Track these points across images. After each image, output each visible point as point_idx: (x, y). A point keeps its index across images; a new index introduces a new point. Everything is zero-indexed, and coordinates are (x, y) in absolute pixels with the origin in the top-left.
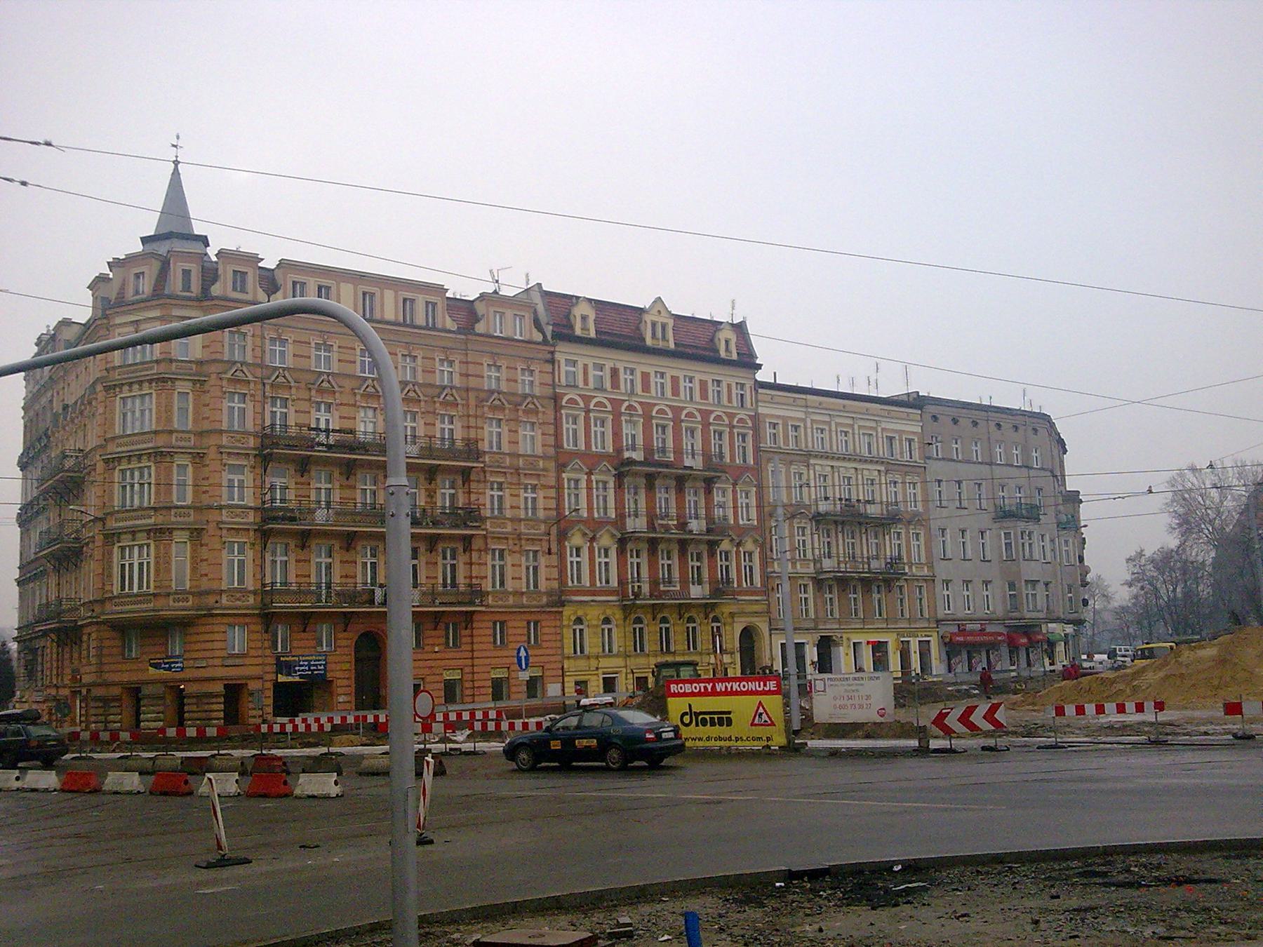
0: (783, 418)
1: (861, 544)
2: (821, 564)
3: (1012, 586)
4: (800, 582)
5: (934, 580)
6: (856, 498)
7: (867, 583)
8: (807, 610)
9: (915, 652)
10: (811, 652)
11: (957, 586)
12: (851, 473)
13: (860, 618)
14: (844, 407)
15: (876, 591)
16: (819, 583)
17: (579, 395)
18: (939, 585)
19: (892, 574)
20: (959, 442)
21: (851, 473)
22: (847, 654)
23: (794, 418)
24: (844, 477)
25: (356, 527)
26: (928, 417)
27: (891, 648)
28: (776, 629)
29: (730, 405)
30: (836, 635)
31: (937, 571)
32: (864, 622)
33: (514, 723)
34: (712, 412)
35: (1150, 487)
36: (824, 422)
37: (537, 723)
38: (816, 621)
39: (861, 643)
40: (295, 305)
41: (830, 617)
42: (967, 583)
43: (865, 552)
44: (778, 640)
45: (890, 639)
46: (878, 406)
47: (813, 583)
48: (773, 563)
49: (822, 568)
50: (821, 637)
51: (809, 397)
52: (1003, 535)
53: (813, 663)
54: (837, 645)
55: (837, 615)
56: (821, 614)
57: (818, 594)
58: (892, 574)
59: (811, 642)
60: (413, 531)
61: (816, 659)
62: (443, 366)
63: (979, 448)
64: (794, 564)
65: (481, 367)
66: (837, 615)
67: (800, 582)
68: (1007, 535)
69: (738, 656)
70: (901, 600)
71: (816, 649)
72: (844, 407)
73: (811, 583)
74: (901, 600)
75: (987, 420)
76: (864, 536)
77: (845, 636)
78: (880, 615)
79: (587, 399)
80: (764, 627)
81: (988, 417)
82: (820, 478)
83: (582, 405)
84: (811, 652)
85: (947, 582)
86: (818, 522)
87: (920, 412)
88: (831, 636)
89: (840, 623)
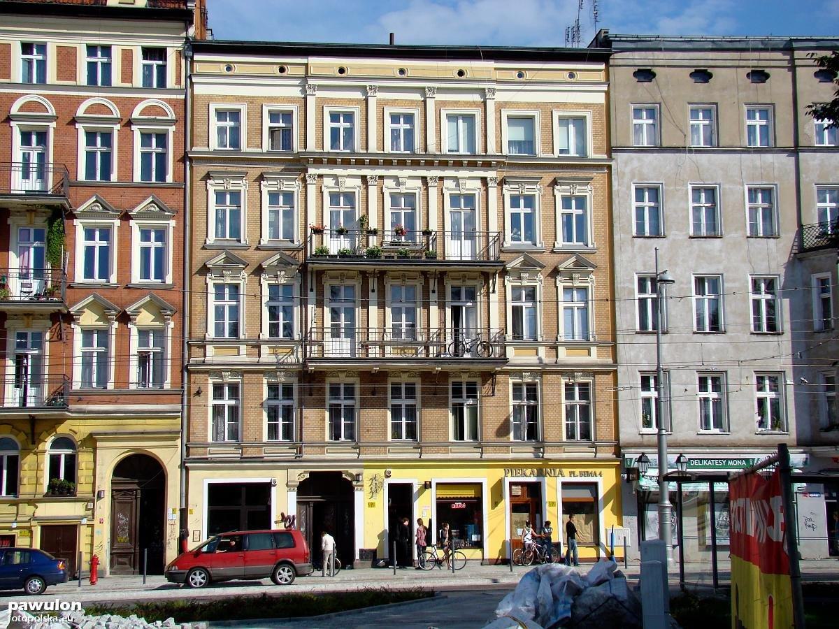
0: (251, 100)
6: (423, 228)
12: (474, 186)
14: (402, 71)
17: (111, 98)
21: (474, 186)
24: (393, 196)
26: (623, 76)
29: (129, 85)
33: (361, 551)
34: (81, 100)
35: (68, 124)
36: (412, 103)
44: (201, 481)
46: (492, 64)
51: (313, 60)
60: (217, 303)
62: (697, 118)
64: (382, 347)
69: (104, 507)
72: (402, 71)
79: (127, 105)
80: (169, 457)
83: (117, 114)
87: (602, 66)
88: (340, 473)
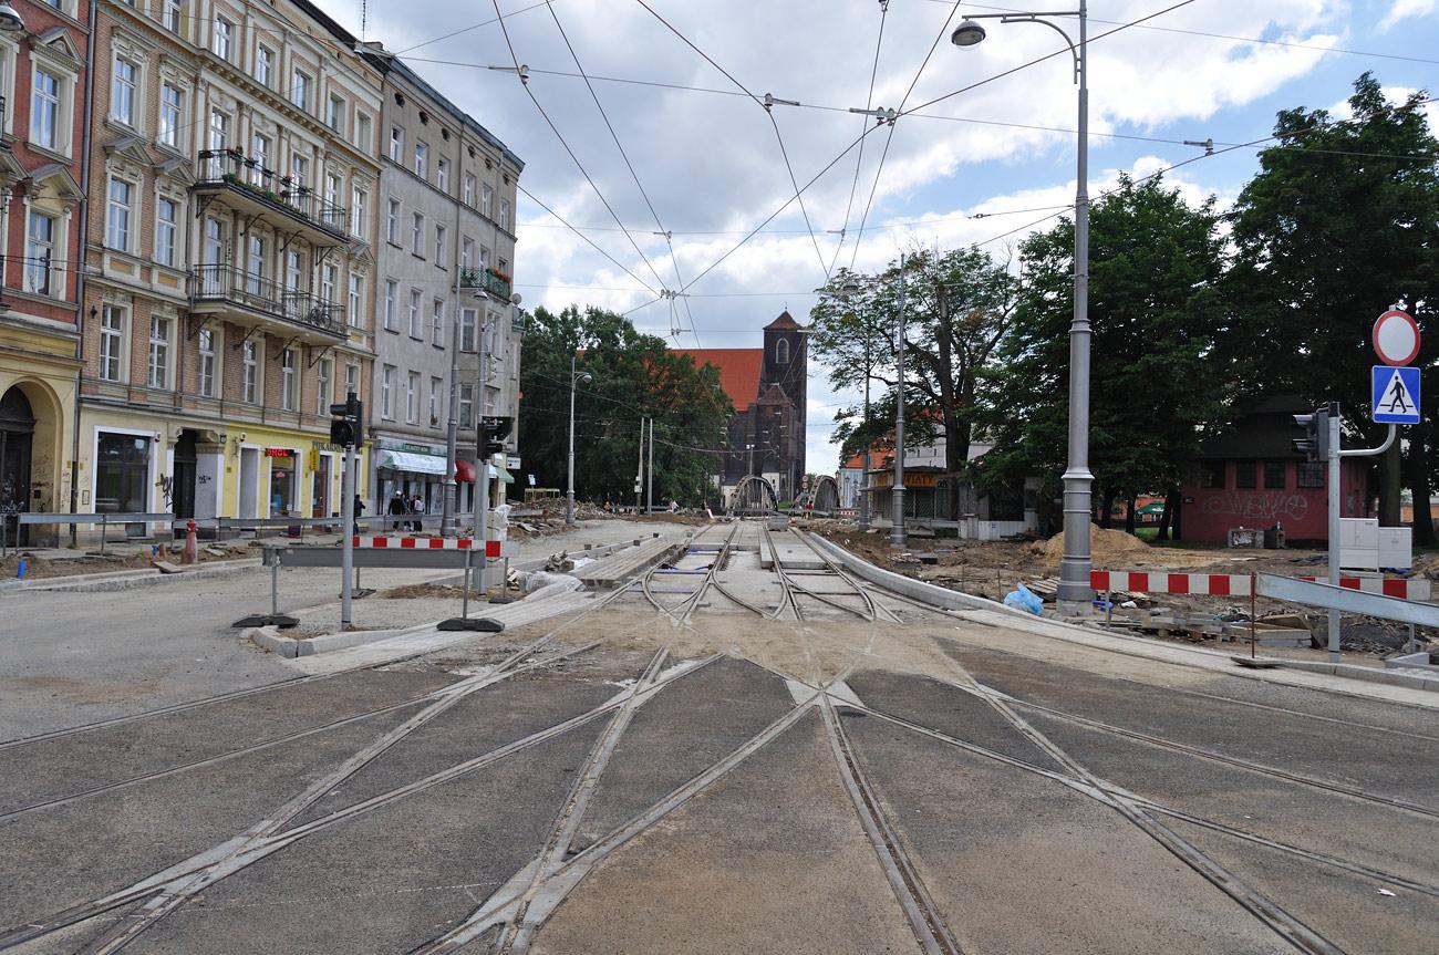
1: (275, 268)
2: (201, 285)
3: (467, 392)
4: (155, 312)
5: (373, 361)
7: (277, 345)
8: (113, 364)
9: (336, 477)
10: (163, 459)
11: (402, 377)
13: (257, 405)
15: (250, 356)
16: (192, 321)
18: (379, 373)
19: (239, 305)
20: (401, 136)
22: (229, 470)
23: (345, 89)
25: (1337, 695)
27: (302, 464)
28: (96, 402)
30: (212, 431)
31: (379, 347)
32: (221, 407)
37: (421, 530)
38: (177, 397)
39: (255, 450)
40: (917, 590)
41: (155, 385)
42: (414, 374)
43: (280, 279)
44: (95, 426)
45: (303, 449)
47: (181, 320)
48: (101, 254)
49: (201, 294)
50: (185, 430)
52: (463, 313)
53: (163, 481)
54: (215, 450)
55: (217, 392)
56: (189, 386)
57: (187, 343)
58: (239, 305)
59: (163, 440)
61: (170, 473)
63: (445, 175)
65: (511, 242)
66: (217, 392)
67: (155, 312)
68: (469, 314)
70: (323, 384)
71: (171, 453)
73: (176, 320)
74: (323, 384)
75: (461, 137)
76: (280, 255)
77: (230, 435)
78: (251, 399)
81: (462, 131)
82: (295, 162)
84: (163, 459)
85: (389, 368)
86: (202, 198)
89: (222, 407)
